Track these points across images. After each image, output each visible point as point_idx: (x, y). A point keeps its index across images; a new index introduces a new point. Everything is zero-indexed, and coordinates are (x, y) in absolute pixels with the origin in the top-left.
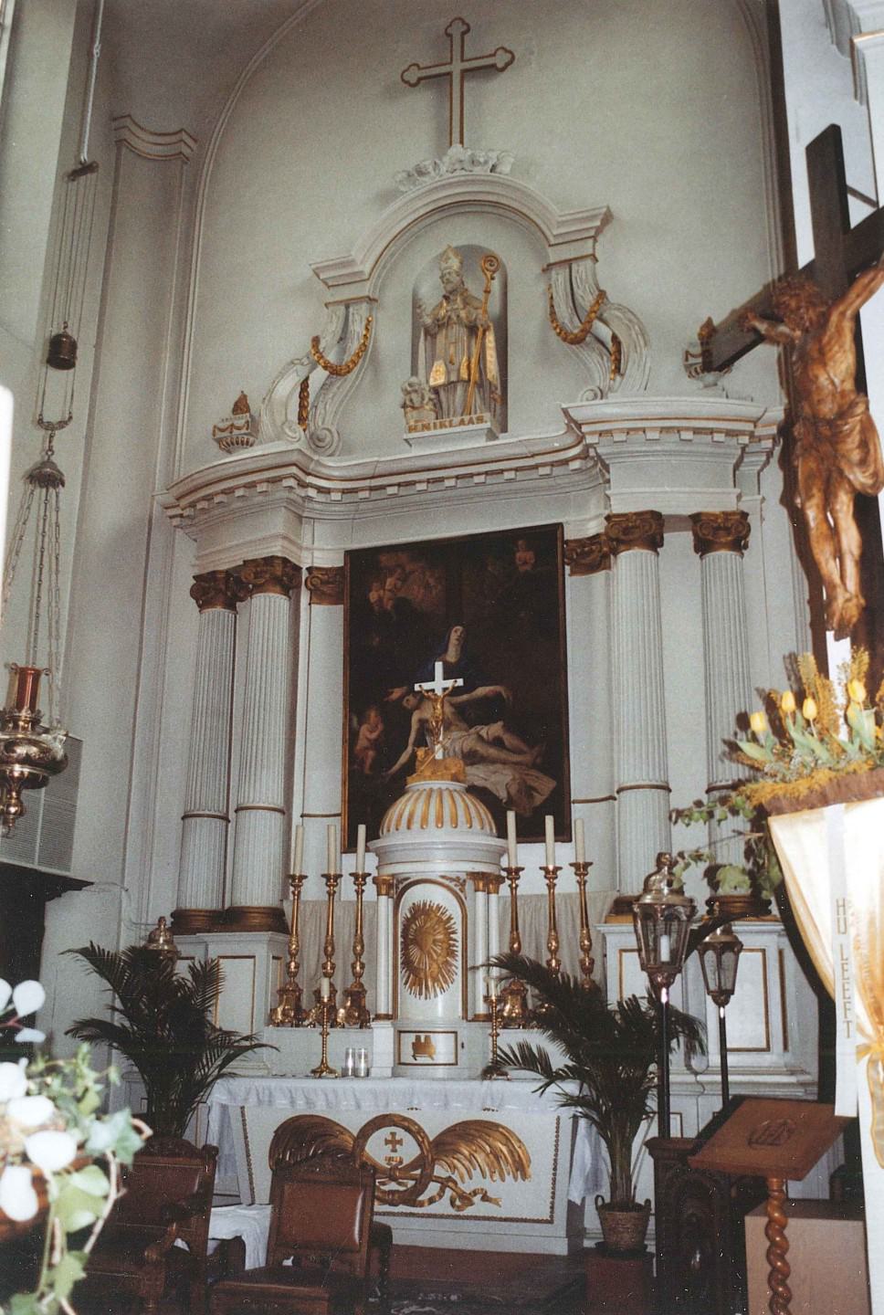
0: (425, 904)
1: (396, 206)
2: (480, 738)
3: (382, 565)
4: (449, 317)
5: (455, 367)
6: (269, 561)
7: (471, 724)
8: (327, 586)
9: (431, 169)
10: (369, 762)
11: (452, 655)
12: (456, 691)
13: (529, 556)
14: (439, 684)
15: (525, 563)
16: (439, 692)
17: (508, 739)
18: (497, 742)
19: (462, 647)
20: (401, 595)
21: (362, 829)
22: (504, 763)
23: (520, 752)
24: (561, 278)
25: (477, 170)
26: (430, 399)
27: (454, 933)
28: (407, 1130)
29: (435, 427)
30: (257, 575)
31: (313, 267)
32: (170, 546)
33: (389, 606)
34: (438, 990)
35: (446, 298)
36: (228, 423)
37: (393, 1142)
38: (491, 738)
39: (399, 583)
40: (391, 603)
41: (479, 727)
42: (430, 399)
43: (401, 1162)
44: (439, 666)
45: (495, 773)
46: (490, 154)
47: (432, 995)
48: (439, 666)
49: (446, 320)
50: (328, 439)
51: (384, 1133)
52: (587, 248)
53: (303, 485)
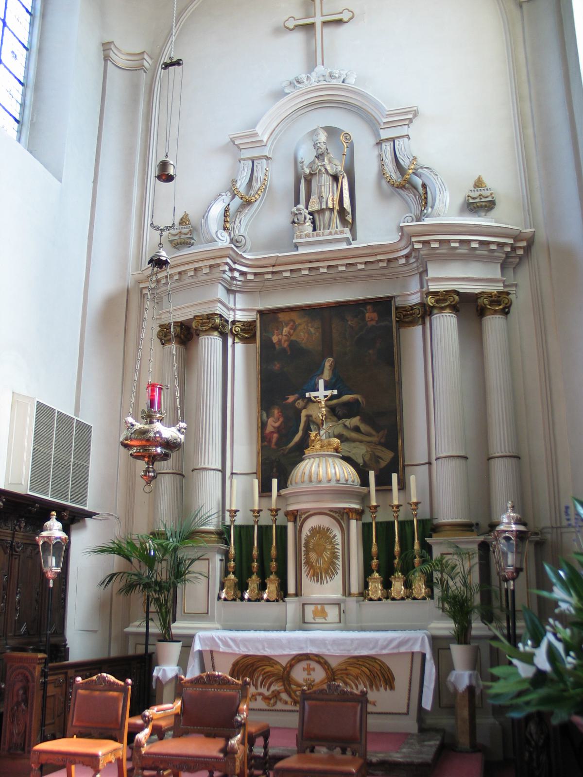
0: (319, 527)
1: (282, 103)
2: (345, 426)
3: (280, 320)
4: (320, 170)
5: (325, 200)
6: (210, 316)
7: (339, 418)
8: (247, 332)
9: (305, 80)
10: (274, 440)
11: (327, 374)
12: (333, 397)
13: (375, 315)
14: (322, 393)
15: (372, 320)
16: (322, 398)
17: (363, 427)
18: (357, 429)
19: (333, 371)
20: (293, 338)
21: (275, 482)
22: (361, 442)
23: (369, 435)
24: (388, 148)
25: (334, 82)
26: (310, 219)
27: (337, 544)
28: (319, 662)
29: (313, 236)
30: (202, 324)
31: (231, 136)
32: (142, 309)
33: (286, 345)
34: (328, 579)
35: (317, 157)
36: (178, 231)
37: (309, 670)
38: (352, 426)
39: (292, 331)
40: (287, 343)
41: (344, 420)
42: (310, 219)
43: (314, 681)
44: (321, 383)
45: (355, 448)
46: (342, 72)
47: (325, 582)
48: (321, 383)
49: (317, 171)
50: (243, 242)
51: (304, 664)
52: (404, 131)
53: (232, 270)
